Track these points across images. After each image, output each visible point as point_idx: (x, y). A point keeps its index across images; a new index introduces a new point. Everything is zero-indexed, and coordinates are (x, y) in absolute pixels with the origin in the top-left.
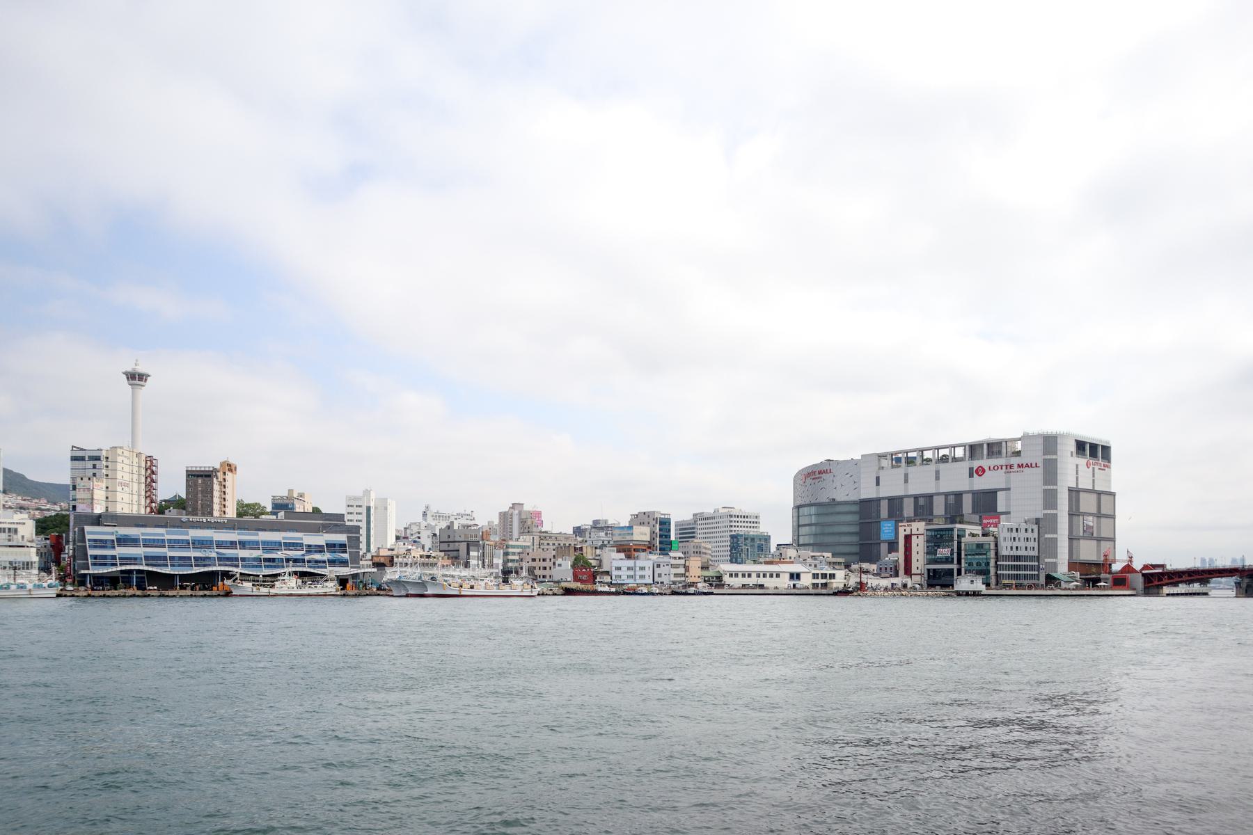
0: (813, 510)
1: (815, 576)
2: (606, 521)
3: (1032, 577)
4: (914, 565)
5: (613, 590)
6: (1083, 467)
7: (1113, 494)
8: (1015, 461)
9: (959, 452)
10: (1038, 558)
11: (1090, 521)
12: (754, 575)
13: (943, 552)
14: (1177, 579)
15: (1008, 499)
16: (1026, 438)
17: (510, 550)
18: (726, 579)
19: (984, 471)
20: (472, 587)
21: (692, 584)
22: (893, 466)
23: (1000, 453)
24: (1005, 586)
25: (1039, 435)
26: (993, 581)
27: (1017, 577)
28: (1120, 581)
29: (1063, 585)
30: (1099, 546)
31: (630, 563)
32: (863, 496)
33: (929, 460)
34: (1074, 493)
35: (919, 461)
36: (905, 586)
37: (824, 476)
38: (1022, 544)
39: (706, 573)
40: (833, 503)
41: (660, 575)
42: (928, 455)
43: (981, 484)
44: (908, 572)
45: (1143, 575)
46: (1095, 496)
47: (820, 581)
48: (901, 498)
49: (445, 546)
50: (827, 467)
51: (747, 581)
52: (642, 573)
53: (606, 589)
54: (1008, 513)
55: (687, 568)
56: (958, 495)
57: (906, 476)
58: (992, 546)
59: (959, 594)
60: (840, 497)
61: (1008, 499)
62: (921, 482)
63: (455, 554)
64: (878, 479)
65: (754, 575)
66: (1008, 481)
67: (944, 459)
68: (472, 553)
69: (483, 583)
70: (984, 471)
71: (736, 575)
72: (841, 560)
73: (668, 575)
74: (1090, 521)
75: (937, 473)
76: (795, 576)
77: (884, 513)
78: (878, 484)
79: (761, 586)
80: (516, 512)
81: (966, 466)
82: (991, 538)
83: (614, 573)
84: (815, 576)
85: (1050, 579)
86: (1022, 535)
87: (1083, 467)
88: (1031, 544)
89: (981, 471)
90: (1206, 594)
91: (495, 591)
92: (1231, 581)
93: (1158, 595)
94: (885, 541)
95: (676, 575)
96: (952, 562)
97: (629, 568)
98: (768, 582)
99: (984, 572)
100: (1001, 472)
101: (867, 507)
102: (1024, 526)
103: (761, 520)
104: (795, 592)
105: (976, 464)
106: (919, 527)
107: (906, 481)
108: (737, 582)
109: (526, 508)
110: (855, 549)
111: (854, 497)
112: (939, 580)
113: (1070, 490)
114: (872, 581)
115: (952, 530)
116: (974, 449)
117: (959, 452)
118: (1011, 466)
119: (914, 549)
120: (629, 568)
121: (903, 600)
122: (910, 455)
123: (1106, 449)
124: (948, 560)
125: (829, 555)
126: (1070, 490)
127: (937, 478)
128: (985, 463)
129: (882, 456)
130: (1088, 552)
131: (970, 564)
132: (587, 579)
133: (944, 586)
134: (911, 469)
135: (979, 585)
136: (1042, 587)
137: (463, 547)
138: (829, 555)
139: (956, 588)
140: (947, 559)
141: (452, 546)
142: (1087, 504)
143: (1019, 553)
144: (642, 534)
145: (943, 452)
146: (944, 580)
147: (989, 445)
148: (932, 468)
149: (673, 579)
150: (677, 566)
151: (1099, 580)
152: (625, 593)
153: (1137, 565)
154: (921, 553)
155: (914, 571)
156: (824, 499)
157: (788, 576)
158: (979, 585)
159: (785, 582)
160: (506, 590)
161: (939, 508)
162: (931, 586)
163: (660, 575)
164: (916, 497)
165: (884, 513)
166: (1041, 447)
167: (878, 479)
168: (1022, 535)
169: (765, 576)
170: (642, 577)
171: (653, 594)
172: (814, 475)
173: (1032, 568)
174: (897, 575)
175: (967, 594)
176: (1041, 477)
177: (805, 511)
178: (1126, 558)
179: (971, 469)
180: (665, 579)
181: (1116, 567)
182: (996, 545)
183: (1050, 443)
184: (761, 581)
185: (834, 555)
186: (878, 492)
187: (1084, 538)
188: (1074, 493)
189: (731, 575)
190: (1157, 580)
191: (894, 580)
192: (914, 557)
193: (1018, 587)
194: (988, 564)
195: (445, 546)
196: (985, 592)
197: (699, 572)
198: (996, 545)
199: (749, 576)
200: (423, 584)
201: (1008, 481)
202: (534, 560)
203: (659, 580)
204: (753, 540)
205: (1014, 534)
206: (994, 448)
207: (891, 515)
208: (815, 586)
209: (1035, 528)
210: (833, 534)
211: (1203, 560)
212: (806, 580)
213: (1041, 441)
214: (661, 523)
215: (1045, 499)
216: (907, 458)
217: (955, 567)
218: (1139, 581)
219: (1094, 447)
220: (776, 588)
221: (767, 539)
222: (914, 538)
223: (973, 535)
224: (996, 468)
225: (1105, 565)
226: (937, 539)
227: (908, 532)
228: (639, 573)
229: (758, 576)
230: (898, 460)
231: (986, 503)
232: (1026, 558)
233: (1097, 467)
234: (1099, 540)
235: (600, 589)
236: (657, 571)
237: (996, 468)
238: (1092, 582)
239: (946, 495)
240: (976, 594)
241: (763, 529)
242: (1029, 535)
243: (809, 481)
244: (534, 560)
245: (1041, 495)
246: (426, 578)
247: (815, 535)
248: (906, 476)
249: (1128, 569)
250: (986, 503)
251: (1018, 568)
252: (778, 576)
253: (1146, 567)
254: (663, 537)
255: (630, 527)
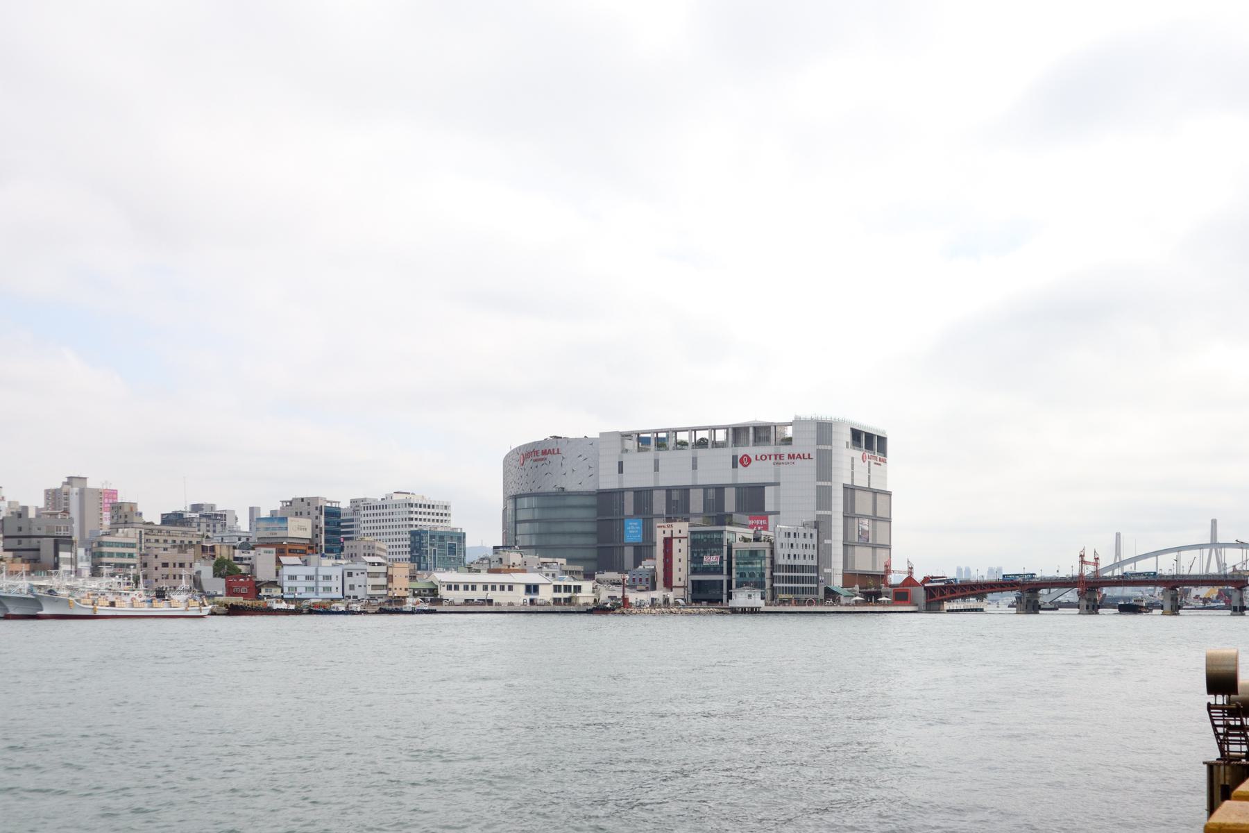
0: (534, 501)
1: (557, 589)
2: (212, 507)
3: (811, 590)
4: (676, 575)
5: (292, 607)
6: (858, 462)
7: (889, 494)
8: (785, 450)
9: (721, 436)
10: (816, 569)
11: (866, 525)
12: (480, 587)
13: (710, 560)
14: (969, 592)
15: (777, 497)
16: (796, 423)
17: (105, 549)
18: (443, 592)
19: (749, 460)
20: (112, 604)
21: (401, 600)
22: (640, 450)
23: (768, 439)
24: (783, 602)
25: (812, 421)
26: (768, 595)
27: (792, 590)
28: (902, 595)
29: (843, 600)
30: (874, 554)
31: (310, 571)
32: (602, 487)
33: (684, 444)
34: (850, 490)
35: (671, 443)
36: (666, 601)
37: (549, 457)
38: (799, 551)
39: (415, 585)
40: (562, 493)
41: (352, 587)
42: (683, 436)
43: (747, 476)
44: (668, 584)
45: (926, 588)
46: (870, 495)
47: (563, 595)
48: (649, 491)
49: (13, 543)
50: (553, 446)
51: (470, 594)
52: (327, 584)
53: (284, 605)
54: (777, 513)
55: (390, 578)
56: (720, 489)
57: (657, 462)
58: (768, 554)
59: (734, 611)
60: (572, 486)
61: (777, 497)
62: (676, 471)
63: (32, 554)
64: (621, 464)
65: (480, 587)
66: (777, 474)
67: (702, 444)
68: (62, 555)
69: (128, 599)
70: (749, 460)
71: (457, 588)
72: (579, 568)
73: (364, 586)
74: (866, 525)
75: (695, 460)
76: (532, 589)
77: (629, 508)
78: (621, 471)
79: (490, 602)
80: (76, 490)
81: (728, 452)
82: (768, 544)
83: (287, 584)
84: (557, 589)
85: (831, 594)
86: (801, 540)
87: (858, 462)
88: (810, 552)
89: (746, 461)
90: (982, 610)
91: (145, 609)
92: (1010, 597)
93: (938, 611)
94: (629, 545)
95: (374, 587)
96: (721, 573)
97: (308, 578)
98: (497, 596)
99: (760, 585)
100: (770, 463)
101: (607, 501)
102: (802, 530)
103: (452, 511)
104: (534, 609)
105: (741, 452)
106: (681, 528)
107: (656, 469)
108: (459, 596)
109: (91, 484)
110: (592, 554)
111: (589, 486)
112: (707, 594)
113: (846, 488)
114: (633, 597)
115: (721, 532)
116: (737, 433)
117: (721, 436)
118: (781, 456)
119: (676, 556)
120: (308, 578)
121: (670, 619)
122: (661, 435)
123: (882, 440)
124: (718, 570)
125: (564, 561)
126: (846, 488)
127: (695, 467)
128: (752, 451)
129: (626, 436)
130: (864, 562)
131: (742, 575)
132: (244, 595)
133: (711, 601)
134: (662, 455)
135: (757, 601)
136: (822, 603)
137: (47, 546)
138: (564, 561)
139: (732, 604)
140: (715, 567)
141: (25, 543)
142: (863, 504)
143: (798, 562)
144: (300, 529)
145: (701, 435)
146: (712, 594)
147: (755, 428)
148: (688, 453)
149: (370, 592)
150: (375, 575)
151: (878, 594)
152: (311, 612)
153: (918, 577)
154: (684, 561)
155: (675, 582)
156: (550, 488)
157: (523, 588)
158: (757, 601)
159: (519, 597)
160: (162, 607)
161: (696, 503)
162: (696, 601)
163: (352, 587)
164: (669, 490)
165: (629, 508)
166: (814, 435)
167: (621, 464)
168: (801, 540)
169: (494, 588)
170: (328, 589)
171: (353, 613)
172: (536, 456)
173: (811, 580)
174: (654, 588)
175: (744, 611)
176: (813, 471)
177: (525, 502)
178: (906, 569)
179: (735, 458)
180: (359, 592)
181: (895, 579)
182: (772, 552)
183: (824, 429)
184: (491, 594)
185: (570, 561)
186: (621, 481)
187: (860, 545)
188: (850, 490)
189: (449, 588)
190: (939, 594)
191: (654, 594)
192: (676, 565)
193: (798, 602)
194: (763, 575)
195: (13, 543)
196: (764, 608)
197: (406, 583)
198: (772, 552)
199: (474, 588)
200: (37, 602)
201: (777, 474)
202: (165, 565)
203: (352, 593)
204: (442, 538)
205: (792, 540)
206: (761, 433)
207: (638, 511)
208: (557, 601)
209: (814, 532)
210: (564, 534)
211: (959, 570)
212: (546, 594)
213: (814, 428)
214: (327, 514)
215: (818, 497)
216: (657, 439)
217: (724, 578)
218: (920, 594)
219: (869, 437)
220: (511, 604)
221: (461, 537)
222: (675, 542)
223: (745, 540)
224: (764, 458)
225: (882, 577)
226: (701, 545)
227: (668, 535)
228: (322, 584)
229: (485, 588)
230: (647, 441)
231: (753, 499)
232: (803, 568)
233: (872, 461)
234: (875, 547)
235: (276, 606)
236: (349, 581)
237: (764, 458)
238: (871, 597)
239: (706, 488)
240: (754, 611)
241: (456, 523)
242: (808, 541)
243: (528, 463)
244: (165, 565)
245: (814, 493)
246: (42, 593)
247: (539, 534)
248: (657, 462)
249: (910, 581)
250: (753, 499)
251: (796, 580)
252: (510, 588)
253: (926, 579)
254: (335, 530)
255: (284, 519)
